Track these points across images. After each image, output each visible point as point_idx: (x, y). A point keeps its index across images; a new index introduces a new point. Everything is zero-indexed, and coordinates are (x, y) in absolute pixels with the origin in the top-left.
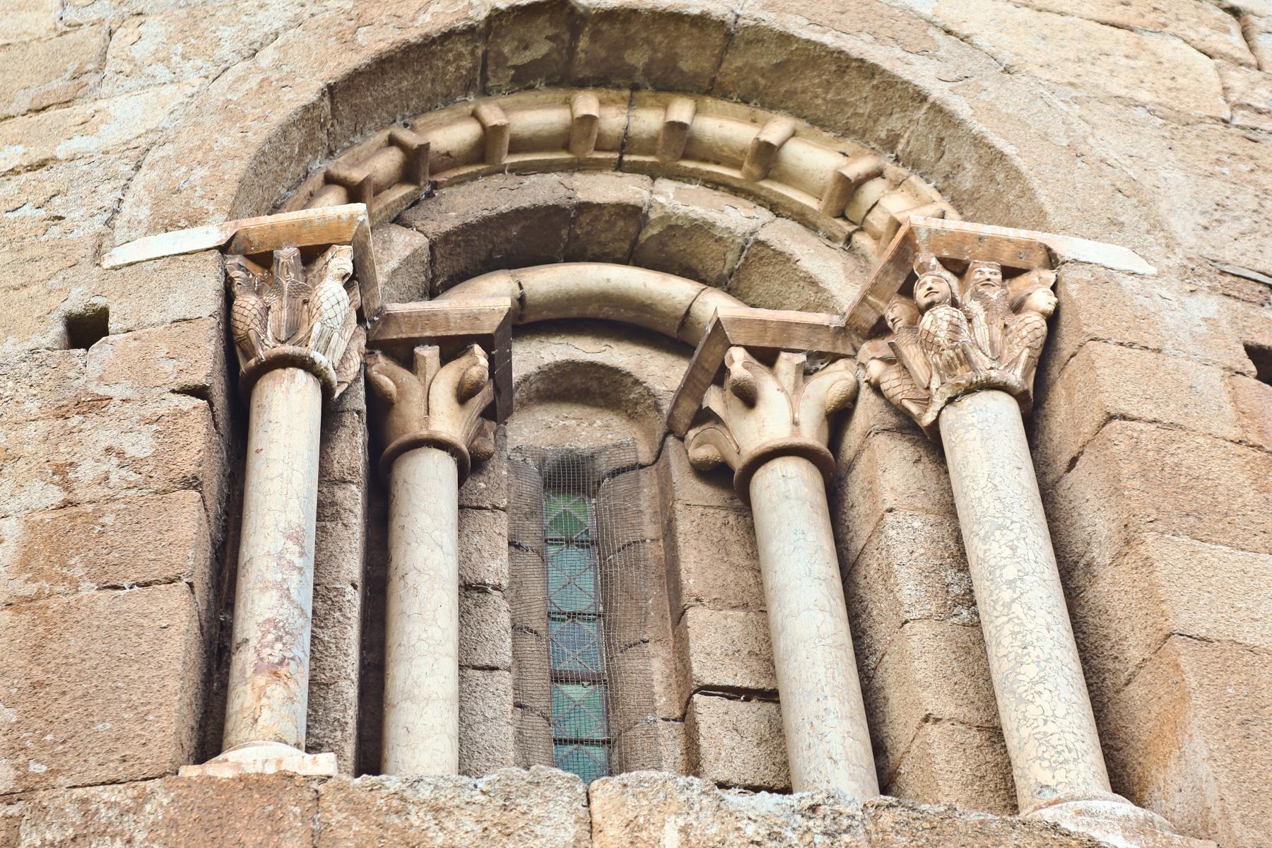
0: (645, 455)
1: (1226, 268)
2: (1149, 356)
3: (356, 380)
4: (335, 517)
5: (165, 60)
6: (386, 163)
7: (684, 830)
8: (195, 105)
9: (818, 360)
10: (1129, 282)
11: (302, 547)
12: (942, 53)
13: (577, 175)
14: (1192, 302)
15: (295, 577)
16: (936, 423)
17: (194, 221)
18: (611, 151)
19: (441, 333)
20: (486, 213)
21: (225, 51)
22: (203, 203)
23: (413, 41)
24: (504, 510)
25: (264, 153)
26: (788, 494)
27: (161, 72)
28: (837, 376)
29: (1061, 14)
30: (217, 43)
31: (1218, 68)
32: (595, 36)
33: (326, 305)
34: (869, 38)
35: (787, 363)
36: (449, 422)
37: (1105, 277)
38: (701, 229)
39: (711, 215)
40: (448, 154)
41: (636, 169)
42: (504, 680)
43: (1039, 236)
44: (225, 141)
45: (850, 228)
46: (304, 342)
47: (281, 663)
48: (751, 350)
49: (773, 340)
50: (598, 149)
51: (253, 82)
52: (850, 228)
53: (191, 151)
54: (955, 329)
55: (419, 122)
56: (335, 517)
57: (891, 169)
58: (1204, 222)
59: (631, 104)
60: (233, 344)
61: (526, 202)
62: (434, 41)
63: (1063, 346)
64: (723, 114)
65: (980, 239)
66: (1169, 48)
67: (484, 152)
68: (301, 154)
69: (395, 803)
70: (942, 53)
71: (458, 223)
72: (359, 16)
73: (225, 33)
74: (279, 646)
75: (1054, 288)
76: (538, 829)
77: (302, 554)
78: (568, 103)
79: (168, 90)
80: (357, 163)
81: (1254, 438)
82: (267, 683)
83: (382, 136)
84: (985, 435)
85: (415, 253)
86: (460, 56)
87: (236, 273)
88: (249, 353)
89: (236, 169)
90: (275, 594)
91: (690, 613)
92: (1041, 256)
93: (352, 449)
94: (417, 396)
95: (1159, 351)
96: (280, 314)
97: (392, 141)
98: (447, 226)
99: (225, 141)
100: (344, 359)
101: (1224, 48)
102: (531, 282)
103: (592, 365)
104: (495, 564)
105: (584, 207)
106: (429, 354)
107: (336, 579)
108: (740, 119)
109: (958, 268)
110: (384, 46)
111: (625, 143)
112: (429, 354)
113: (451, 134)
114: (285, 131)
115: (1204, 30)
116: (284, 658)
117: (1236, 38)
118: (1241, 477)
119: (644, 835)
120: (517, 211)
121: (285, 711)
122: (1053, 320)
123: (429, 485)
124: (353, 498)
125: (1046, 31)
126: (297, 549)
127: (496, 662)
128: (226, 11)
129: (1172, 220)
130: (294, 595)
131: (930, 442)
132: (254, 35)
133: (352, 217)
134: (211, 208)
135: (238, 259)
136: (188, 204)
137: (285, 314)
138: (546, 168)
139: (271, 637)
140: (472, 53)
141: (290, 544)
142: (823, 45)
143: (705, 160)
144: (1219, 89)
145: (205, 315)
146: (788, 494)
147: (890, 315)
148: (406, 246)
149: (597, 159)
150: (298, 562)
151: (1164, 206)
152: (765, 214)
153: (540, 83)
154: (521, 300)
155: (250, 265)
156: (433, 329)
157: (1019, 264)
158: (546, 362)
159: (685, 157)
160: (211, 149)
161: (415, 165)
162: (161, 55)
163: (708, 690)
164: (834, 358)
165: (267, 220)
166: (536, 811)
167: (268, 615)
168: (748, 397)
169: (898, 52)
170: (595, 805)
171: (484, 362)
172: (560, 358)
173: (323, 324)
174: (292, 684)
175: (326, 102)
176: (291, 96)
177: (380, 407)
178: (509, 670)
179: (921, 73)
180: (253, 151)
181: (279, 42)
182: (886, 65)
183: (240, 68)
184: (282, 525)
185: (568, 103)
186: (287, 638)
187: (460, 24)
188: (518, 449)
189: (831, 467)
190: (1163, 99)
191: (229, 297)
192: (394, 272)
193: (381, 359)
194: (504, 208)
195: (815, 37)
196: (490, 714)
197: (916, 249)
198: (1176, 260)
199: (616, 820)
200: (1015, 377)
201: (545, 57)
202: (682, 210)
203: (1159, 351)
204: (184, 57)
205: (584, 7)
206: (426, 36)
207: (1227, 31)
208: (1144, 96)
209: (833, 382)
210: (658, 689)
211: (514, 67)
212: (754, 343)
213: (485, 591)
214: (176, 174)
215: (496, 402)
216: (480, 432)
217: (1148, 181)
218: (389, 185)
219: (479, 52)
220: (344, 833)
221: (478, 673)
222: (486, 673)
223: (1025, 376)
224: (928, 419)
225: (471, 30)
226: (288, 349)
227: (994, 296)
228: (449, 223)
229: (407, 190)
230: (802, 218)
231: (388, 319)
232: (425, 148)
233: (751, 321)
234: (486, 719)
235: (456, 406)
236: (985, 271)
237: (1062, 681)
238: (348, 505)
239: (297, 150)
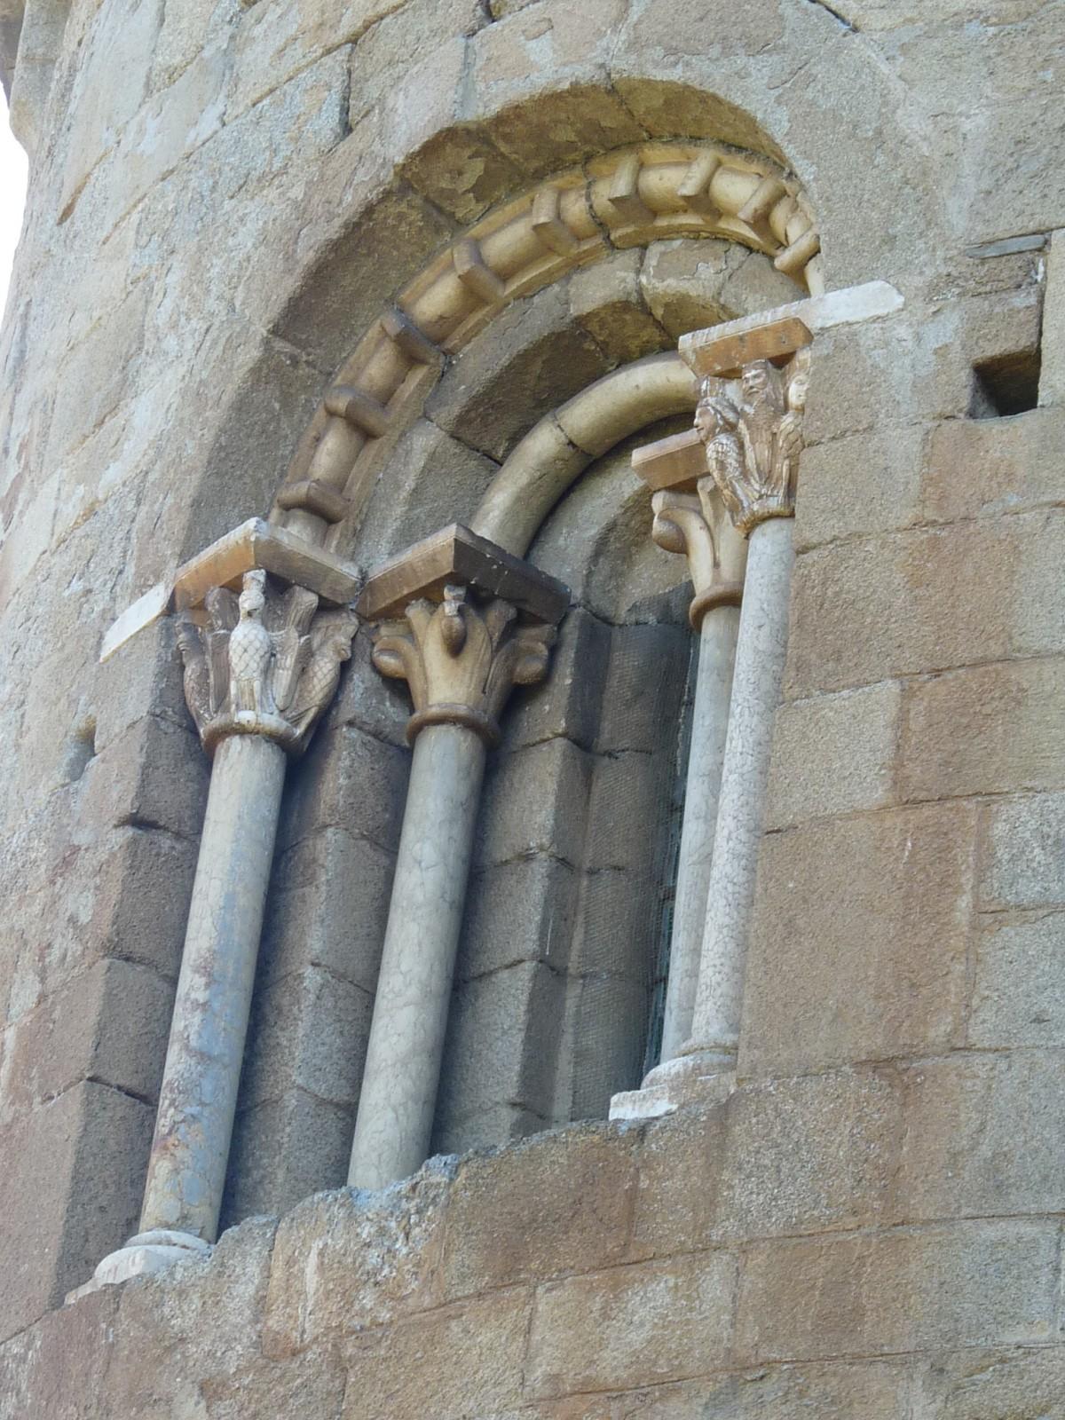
6: (377, 366)
19: (415, 587)
20: (489, 375)
23: (335, 237)
25: (221, 448)
32: (507, 138)
40: (441, 317)
46: (227, 710)
49: (687, 471)
50: (579, 238)
62: (357, 225)
63: (323, 794)
65: (741, 339)
68: (284, 404)
86: (401, 217)
92: (799, 335)
94: (416, 668)
102: (570, 422)
105: (580, 321)
111: (601, 225)
120: (519, 356)
133: (246, 540)
138: (544, 283)
140: (410, 206)
149: (585, 252)
153: (501, 192)
156: (408, 585)
157: (785, 349)
158: (626, 496)
173: (238, 681)
201: (486, 170)
205: (475, 122)
211: (468, 191)
212: (670, 483)
218: (400, 379)
219: (418, 201)
225: (387, 194)
229: (420, 374)
233: (660, 459)
235: (451, 661)
239: (277, 406)
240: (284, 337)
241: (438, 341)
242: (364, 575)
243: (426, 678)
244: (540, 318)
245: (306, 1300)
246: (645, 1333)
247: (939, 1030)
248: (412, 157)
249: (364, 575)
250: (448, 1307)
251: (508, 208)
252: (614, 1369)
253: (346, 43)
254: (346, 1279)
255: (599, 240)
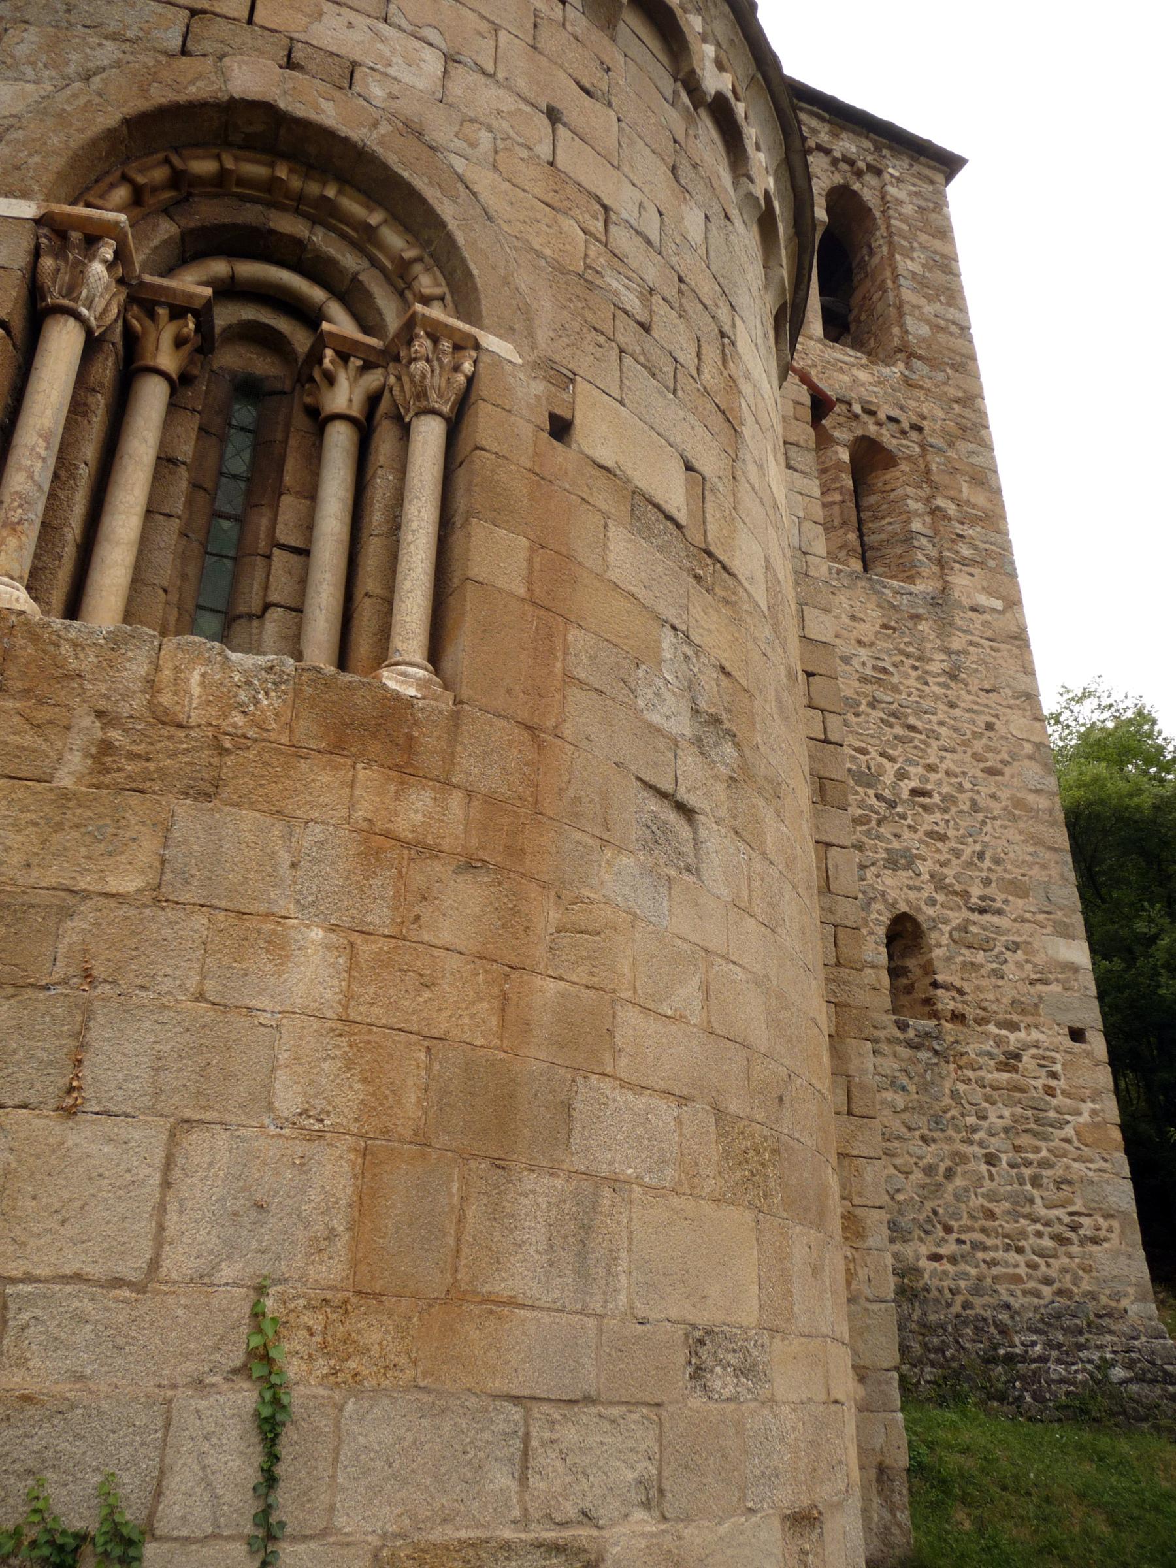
0: (287, 388)
1: (554, 366)
2: (505, 413)
3: (116, 320)
4: (85, 414)
5: (33, 64)
6: (159, 174)
7: (203, 675)
8: (42, 108)
9: (367, 367)
10: (508, 367)
11: (48, 443)
12: (460, 200)
13: (273, 210)
14: (533, 384)
15: (39, 464)
16: (410, 423)
17: (25, 195)
18: (292, 200)
19: (170, 301)
21: (71, 70)
22: (32, 182)
24: (199, 412)
25: (78, 155)
26: (340, 438)
27: (29, 70)
28: (376, 377)
29: (524, 190)
30: (67, 63)
31: (586, 241)
33: (91, 279)
34: (426, 180)
35: (355, 362)
36: (167, 359)
37: (498, 361)
38: (332, 262)
39: (339, 257)
41: (305, 216)
42: (176, 524)
43: (474, 330)
44: (55, 140)
45: (404, 286)
46: (76, 300)
47: (18, 523)
48: (337, 352)
51: (82, 101)
52: (404, 286)
53: (33, 140)
54: (424, 376)
55: (185, 152)
56: (85, 414)
57: (427, 259)
58: (552, 334)
59: (307, 177)
60: (34, 290)
61: (239, 220)
62: (195, 106)
64: (350, 198)
66: (569, 225)
67: (221, 181)
69: (54, 637)
70: (460, 200)
71: (198, 224)
72: (155, 73)
73: (74, 57)
74: (20, 511)
75: (475, 362)
76: (128, 665)
77: (47, 448)
78: (272, 165)
79: (31, 87)
80: (141, 171)
81: (537, 469)
82: (8, 536)
83: (160, 156)
84: (429, 435)
85: (170, 238)
87: (43, 240)
88: (44, 299)
89: (57, 163)
90: (24, 474)
91: (283, 497)
92: (472, 343)
93: (106, 370)
94: (152, 337)
95: (509, 411)
96: (65, 277)
97: (167, 161)
98: (192, 225)
99: (55, 140)
100: (106, 309)
101: (592, 229)
103: (268, 326)
104: (185, 448)
106: (162, 312)
107: (76, 458)
108: (361, 204)
109: (435, 340)
110: (164, 101)
111: (301, 198)
112: (162, 312)
113: (203, 167)
114: (94, 143)
115: (587, 216)
116: (21, 519)
117: (600, 225)
118: (524, 491)
119: (182, 675)
121: (15, 555)
122: (470, 380)
123: (152, 398)
124: (100, 403)
125: (514, 200)
126: (45, 444)
127: (174, 511)
128: (77, 40)
129: (539, 332)
130: (36, 477)
131: (405, 430)
132: (91, 65)
134: (36, 188)
135: (45, 231)
136: (23, 180)
137: (67, 278)
139: (16, 504)
141: (40, 441)
142: (402, 177)
143: (341, 222)
144: (583, 255)
145: (16, 267)
146: (340, 438)
147: (402, 355)
148: (167, 231)
150: (43, 453)
151: (537, 322)
152: (366, 264)
154: (233, 277)
155: (53, 236)
157: (462, 343)
159: (332, 216)
160: (45, 144)
161: (178, 179)
162: (31, 59)
163: (282, 547)
164: (376, 366)
165: (67, 209)
166: (130, 654)
167: (18, 488)
168: (331, 380)
169: (439, 194)
170: (163, 653)
171: (192, 326)
172: (251, 317)
174: (23, 538)
175: (124, 128)
176: (101, 119)
177: (131, 340)
178: (179, 518)
179: (447, 211)
180: (71, 153)
181: (104, 75)
182: (431, 201)
183: (77, 85)
184: (38, 426)
185: (272, 165)
186: (26, 506)
187: (211, 100)
188: (221, 368)
189: (365, 430)
190: (556, 256)
191: (36, 253)
192: (156, 248)
193: (135, 307)
194: (227, 221)
195: (400, 171)
196: (162, 545)
197: (416, 324)
198: (533, 357)
199: (170, 665)
200: (446, 409)
202: (324, 248)
203: (509, 411)
204: (45, 66)
206: (190, 102)
207: (598, 219)
208: (548, 252)
209: (373, 379)
210: (262, 536)
213: (176, 464)
214: (21, 155)
215: (204, 344)
216: (191, 362)
217: (535, 305)
220: (22, 653)
221: (162, 517)
222: (166, 518)
223: (452, 409)
224: (407, 420)
226: (66, 302)
227: (446, 361)
228: (193, 222)
230: (382, 269)
231: (142, 284)
232: (184, 172)
234: (160, 548)
236: (446, 345)
237: (420, 593)
238: (93, 407)
240: (129, 127)
241: (190, 185)
242: (466, 376)
243: (157, 349)
244: (251, 215)
245: (191, 699)
246: (420, 817)
247: (550, 723)
248: (243, 100)
249: (466, 376)
250: (298, 752)
251: (258, 156)
252: (404, 831)
253: (187, 8)
254: (221, 698)
255: (294, 204)
